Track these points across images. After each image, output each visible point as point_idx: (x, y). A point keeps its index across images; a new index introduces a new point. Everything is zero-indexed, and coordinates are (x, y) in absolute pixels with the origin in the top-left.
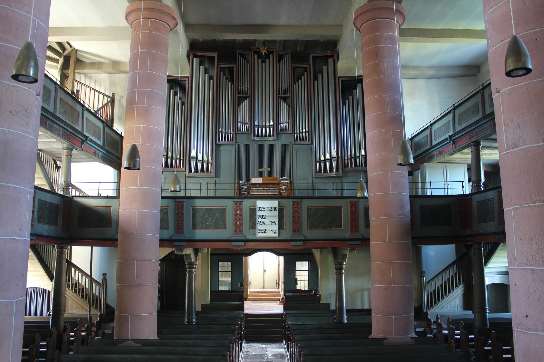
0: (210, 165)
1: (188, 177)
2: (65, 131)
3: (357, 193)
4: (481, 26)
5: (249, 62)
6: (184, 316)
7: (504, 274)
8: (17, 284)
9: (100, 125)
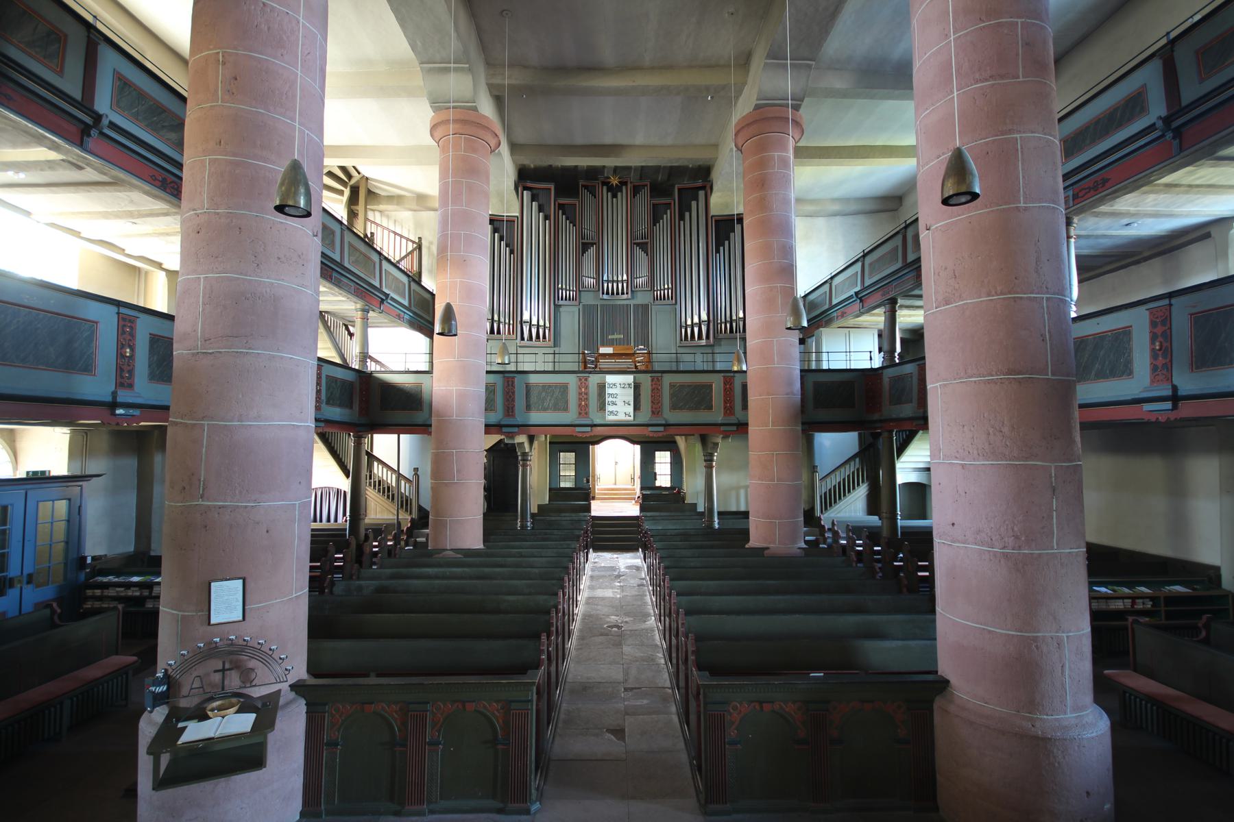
0: (547, 331)
1: (520, 347)
2: (358, 287)
3: (733, 365)
4: (910, 140)
5: (595, 197)
6: (517, 520)
7: (910, 470)
8: (300, 483)
9: (405, 279)
